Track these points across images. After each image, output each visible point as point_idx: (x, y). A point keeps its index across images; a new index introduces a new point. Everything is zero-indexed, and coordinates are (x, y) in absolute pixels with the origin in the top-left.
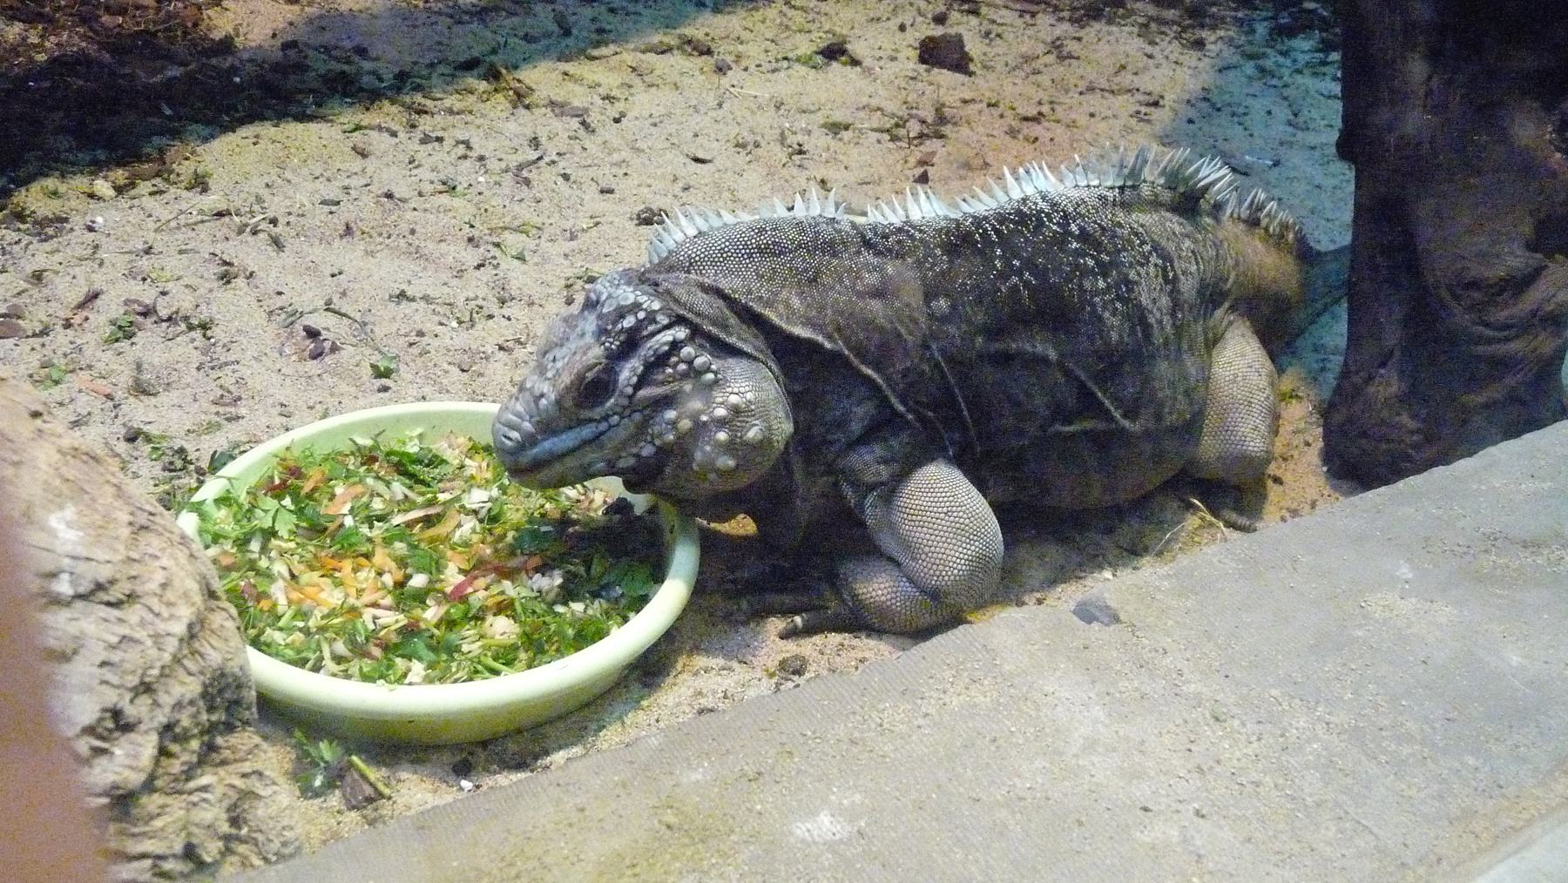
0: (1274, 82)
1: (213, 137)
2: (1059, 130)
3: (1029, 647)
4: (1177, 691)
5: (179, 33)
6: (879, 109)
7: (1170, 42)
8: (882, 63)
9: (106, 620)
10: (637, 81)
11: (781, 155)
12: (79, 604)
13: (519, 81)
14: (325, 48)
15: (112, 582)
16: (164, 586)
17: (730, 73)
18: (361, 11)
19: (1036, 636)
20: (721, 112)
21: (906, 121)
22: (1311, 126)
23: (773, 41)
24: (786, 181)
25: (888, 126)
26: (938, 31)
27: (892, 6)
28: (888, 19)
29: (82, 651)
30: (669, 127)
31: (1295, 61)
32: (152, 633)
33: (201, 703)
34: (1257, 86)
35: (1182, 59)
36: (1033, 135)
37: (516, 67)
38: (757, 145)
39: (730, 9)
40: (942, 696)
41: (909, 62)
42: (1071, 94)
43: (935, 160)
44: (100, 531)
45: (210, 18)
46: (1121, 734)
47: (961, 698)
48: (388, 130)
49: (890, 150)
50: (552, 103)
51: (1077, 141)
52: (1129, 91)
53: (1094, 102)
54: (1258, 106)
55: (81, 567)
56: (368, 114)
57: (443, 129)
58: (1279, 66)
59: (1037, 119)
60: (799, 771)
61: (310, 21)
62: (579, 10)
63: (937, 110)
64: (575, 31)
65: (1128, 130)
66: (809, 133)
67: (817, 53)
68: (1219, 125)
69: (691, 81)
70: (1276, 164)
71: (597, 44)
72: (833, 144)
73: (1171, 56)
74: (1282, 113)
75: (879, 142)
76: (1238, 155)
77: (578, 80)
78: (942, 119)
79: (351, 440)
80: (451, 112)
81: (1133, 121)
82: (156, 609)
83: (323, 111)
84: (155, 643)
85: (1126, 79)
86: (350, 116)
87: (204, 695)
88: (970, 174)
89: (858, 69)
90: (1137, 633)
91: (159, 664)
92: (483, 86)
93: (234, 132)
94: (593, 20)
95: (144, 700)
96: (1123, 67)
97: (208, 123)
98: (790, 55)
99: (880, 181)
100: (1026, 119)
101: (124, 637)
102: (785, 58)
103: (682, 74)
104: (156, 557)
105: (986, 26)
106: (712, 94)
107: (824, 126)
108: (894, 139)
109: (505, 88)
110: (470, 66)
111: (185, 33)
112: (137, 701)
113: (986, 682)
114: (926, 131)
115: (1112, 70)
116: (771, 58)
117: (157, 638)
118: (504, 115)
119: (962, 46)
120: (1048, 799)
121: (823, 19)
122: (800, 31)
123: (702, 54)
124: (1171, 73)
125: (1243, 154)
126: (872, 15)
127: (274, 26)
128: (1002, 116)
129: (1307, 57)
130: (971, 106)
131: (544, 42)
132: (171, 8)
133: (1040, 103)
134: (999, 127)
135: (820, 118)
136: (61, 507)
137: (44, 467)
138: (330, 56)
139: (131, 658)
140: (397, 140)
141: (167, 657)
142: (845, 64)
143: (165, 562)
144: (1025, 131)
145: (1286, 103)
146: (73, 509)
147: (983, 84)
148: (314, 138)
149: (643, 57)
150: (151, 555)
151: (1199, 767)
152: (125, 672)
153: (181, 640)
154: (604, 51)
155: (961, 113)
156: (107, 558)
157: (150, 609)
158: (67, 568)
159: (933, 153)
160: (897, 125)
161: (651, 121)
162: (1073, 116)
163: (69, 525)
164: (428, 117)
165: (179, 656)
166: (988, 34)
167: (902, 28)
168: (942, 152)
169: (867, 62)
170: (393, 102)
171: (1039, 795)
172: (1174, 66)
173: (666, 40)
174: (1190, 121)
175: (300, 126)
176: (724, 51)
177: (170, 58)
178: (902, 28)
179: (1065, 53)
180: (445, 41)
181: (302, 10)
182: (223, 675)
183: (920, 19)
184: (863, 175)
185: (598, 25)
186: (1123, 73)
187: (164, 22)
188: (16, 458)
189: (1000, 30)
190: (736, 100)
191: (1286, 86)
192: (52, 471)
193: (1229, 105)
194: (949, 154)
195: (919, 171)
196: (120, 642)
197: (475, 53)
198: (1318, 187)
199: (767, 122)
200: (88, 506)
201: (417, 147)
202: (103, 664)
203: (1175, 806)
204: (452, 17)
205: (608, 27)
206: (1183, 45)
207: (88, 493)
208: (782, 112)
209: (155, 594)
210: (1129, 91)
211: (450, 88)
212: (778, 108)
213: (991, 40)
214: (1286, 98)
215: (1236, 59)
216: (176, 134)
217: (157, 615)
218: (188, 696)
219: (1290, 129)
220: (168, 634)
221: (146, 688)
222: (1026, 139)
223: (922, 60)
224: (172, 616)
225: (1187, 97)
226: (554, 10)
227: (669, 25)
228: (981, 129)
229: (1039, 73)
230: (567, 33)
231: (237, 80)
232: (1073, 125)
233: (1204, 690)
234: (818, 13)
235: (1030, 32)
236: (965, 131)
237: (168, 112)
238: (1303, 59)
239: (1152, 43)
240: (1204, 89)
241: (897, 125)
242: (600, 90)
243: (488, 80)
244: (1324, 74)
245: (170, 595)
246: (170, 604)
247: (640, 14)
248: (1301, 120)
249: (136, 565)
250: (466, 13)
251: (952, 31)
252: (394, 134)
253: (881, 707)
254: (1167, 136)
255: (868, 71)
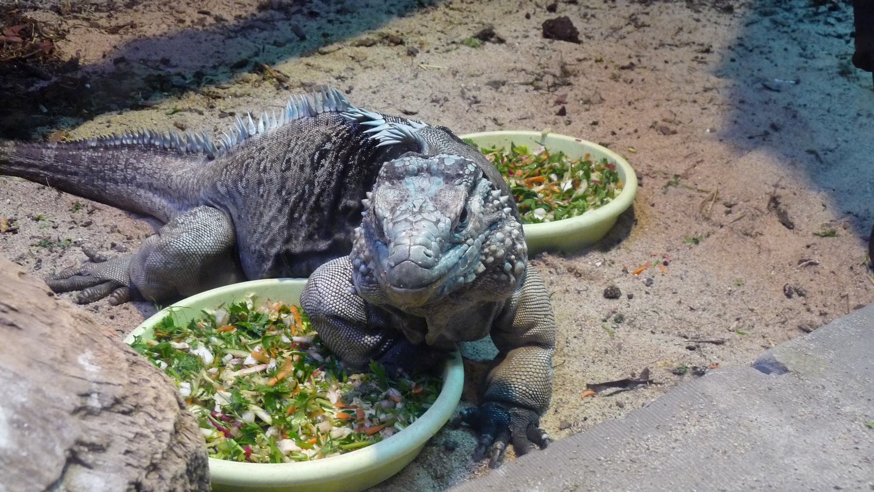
0: (785, 29)
1: (78, 124)
2: (647, 74)
3: (733, 392)
4: (838, 412)
5: (41, 58)
6: (523, 70)
7: (709, 10)
8: (519, 40)
9: (123, 423)
10: (357, 66)
11: (465, 105)
12: (105, 414)
13: (279, 72)
14: (144, 60)
15: (124, 398)
16: (156, 399)
17: (418, 55)
18: (161, 36)
19: (736, 385)
20: (417, 81)
21: (543, 76)
22: (816, 55)
23: (442, 32)
24: (471, 121)
25: (531, 81)
26: (553, 16)
27: (518, 3)
28: (517, 11)
29: (113, 444)
30: (385, 94)
31: (796, 14)
32: (153, 430)
33: (186, 477)
34: (774, 33)
35: (719, 20)
36: (629, 78)
37: (274, 64)
38: (446, 100)
39: (410, 14)
40: (684, 427)
41: (537, 38)
42: (649, 50)
43: (567, 100)
44: (110, 363)
45: (59, 48)
46: (808, 441)
47: (697, 427)
48: (196, 111)
49: (535, 96)
50: (303, 85)
51: (660, 79)
52: (688, 44)
53: (666, 53)
54: (777, 45)
55: (104, 389)
56: (180, 102)
57: (233, 107)
58: (787, 19)
59: (631, 67)
60: (602, 483)
61: (128, 45)
62: (307, 23)
63: (562, 67)
64: (308, 37)
65: (691, 70)
66: (479, 89)
67: (475, 37)
68: (753, 61)
69: (393, 62)
70: (798, 82)
71: (326, 44)
72: (497, 95)
73: (711, 19)
74: (795, 49)
75: (527, 91)
76: (770, 79)
77: (318, 68)
78: (566, 73)
79: (204, 312)
80: (235, 96)
81: (695, 64)
82: (154, 414)
83: (149, 102)
84: (156, 436)
85: (684, 37)
86: (168, 104)
87: (189, 472)
88: (592, 107)
89: (504, 45)
90: (802, 377)
91: (160, 451)
92: (255, 77)
93: (92, 120)
94: (319, 28)
95: (154, 476)
96: (681, 29)
97: (73, 115)
98: (456, 40)
99: (532, 117)
100: (623, 68)
101: (137, 434)
102: (454, 42)
103: (386, 58)
104: (148, 381)
105: (583, 10)
106: (408, 70)
107: (488, 84)
108: (537, 89)
109: (270, 78)
110: (241, 65)
111: (45, 58)
112: (149, 476)
113: (710, 416)
114: (557, 82)
115: (673, 32)
116: (443, 43)
117: (157, 432)
118: (272, 95)
119: (571, 24)
120: (771, 486)
121: (474, 15)
122: (460, 24)
123: (397, 44)
124: (714, 30)
125: (773, 78)
126: (506, 10)
127: (104, 49)
128: (606, 68)
129: (804, 12)
130: (584, 63)
131: (288, 45)
132: (33, 43)
133: (630, 57)
134: (606, 75)
135: (484, 79)
136: (83, 352)
137: (68, 326)
138: (148, 66)
139: (143, 446)
140: (204, 117)
141: (164, 446)
142: (494, 43)
143: (153, 383)
144: (624, 76)
145: (796, 43)
146: (90, 352)
147: (589, 48)
148: (148, 120)
149: (358, 49)
150: (143, 380)
151: (866, 459)
152: (141, 457)
153: (171, 434)
154: (330, 48)
155: (578, 68)
156: (119, 382)
157: (151, 416)
158: (96, 390)
159: (565, 96)
160: (537, 80)
161: (371, 90)
162: (654, 64)
163: (91, 362)
164: (221, 100)
165: (171, 445)
166: (585, 15)
167: (528, 16)
168: (571, 95)
169: (509, 40)
170: (196, 92)
171: (764, 485)
172: (715, 25)
173: (371, 37)
174: (733, 60)
175: (136, 113)
176: (411, 41)
177: (41, 77)
178: (528, 16)
179: (640, 23)
180: (222, 51)
181: (122, 37)
182: (196, 458)
183: (538, 10)
184: (522, 113)
185: (322, 31)
186: (681, 33)
187: (29, 51)
188: (50, 321)
189: (593, 12)
190: (426, 72)
191: (794, 31)
192: (73, 329)
193: (757, 47)
194: (576, 95)
195: (558, 108)
196: (135, 437)
197: (244, 55)
198: (829, 95)
199: (449, 86)
200: (99, 350)
201: (218, 120)
202: (127, 452)
203: (856, 484)
204: (222, 34)
205: (330, 32)
206: (718, 11)
207: (96, 342)
208: (457, 77)
209: (152, 405)
210: (688, 44)
211: (232, 80)
212: (454, 75)
213: (588, 19)
214: (795, 39)
215: (756, 17)
216: (53, 124)
217: (154, 418)
218: (180, 472)
219: (803, 59)
220: (164, 431)
221: (154, 467)
222: (625, 81)
223: (545, 36)
224: (164, 419)
225: (727, 45)
226: (290, 25)
227: (370, 28)
228: (594, 78)
229: (625, 37)
230: (303, 38)
231: (88, 86)
232: (654, 69)
233: (856, 409)
234: (470, 11)
235: (614, 11)
236: (582, 80)
237: (45, 110)
238: (801, 12)
239: (698, 12)
240: (738, 38)
241: (537, 80)
242: (334, 73)
243: (257, 73)
244: (819, 21)
245: (161, 405)
246: (161, 411)
247: (350, 23)
248: (808, 52)
249: (136, 386)
250: (232, 31)
251: (562, 15)
252: (201, 113)
253: (645, 438)
254: (719, 71)
255: (511, 46)
